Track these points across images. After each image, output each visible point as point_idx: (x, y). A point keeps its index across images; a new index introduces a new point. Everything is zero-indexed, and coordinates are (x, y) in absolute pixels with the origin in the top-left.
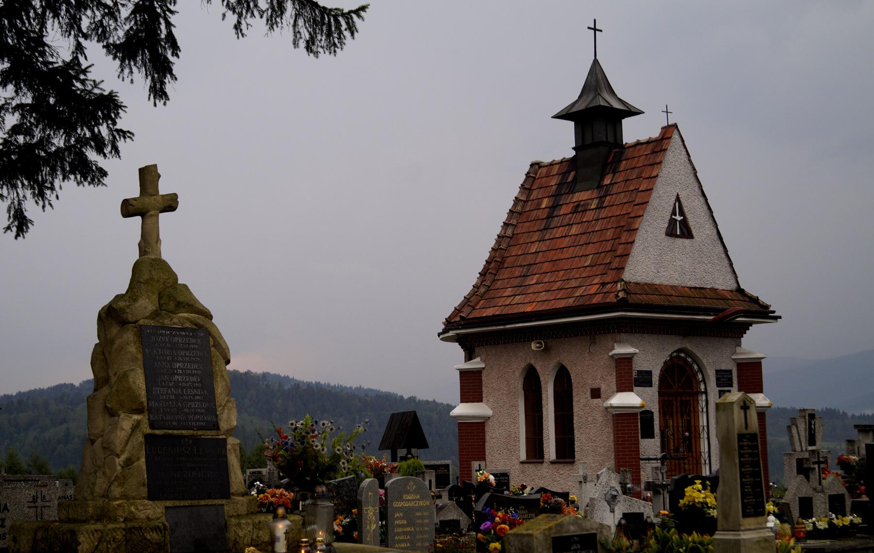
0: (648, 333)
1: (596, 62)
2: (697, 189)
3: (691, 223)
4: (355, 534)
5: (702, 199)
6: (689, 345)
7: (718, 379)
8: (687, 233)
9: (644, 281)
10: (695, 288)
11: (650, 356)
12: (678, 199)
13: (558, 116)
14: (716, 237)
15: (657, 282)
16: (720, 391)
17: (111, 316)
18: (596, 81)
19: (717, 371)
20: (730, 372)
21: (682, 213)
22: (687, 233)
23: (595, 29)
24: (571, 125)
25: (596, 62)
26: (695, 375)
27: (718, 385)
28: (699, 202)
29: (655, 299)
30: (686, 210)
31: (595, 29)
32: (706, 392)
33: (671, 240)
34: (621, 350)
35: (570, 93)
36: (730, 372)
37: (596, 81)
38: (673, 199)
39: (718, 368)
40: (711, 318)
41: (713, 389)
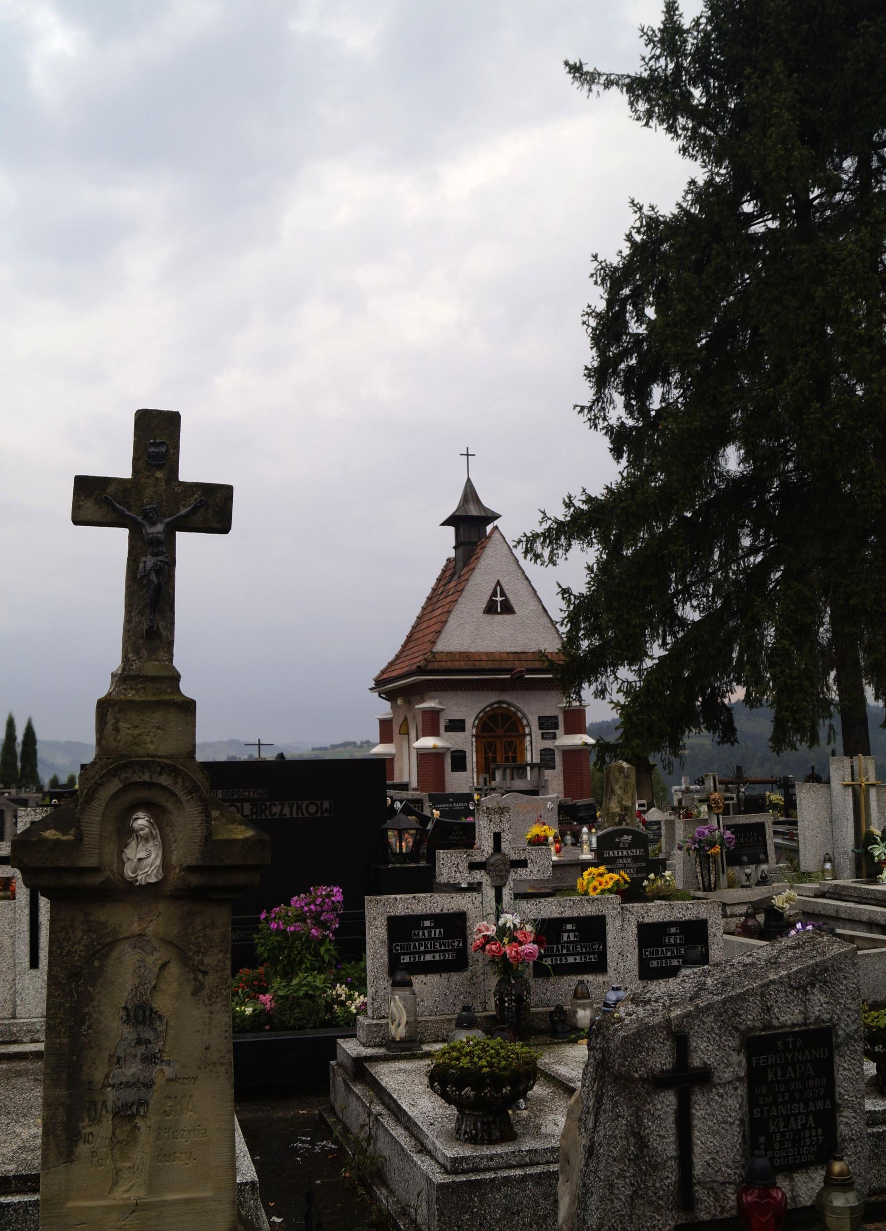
0: (461, 690)
1: (469, 480)
2: (520, 574)
3: (513, 602)
4: (762, 856)
5: (526, 582)
6: (507, 697)
7: (540, 724)
8: (507, 609)
9: (458, 650)
10: (516, 653)
11: (468, 708)
12: (498, 583)
13: (442, 524)
14: (542, 610)
15: (473, 650)
16: (543, 734)
17: (103, 706)
18: (470, 494)
19: (540, 718)
20: (556, 718)
21: (503, 594)
22: (507, 609)
23: (468, 455)
24: (451, 530)
25: (469, 480)
26: (520, 720)
27: (540, 729)
28: (522, 585)
29: (463, 665)
30: (507, 592)
31: (468, 455)
32: (530, 734)
33: (489, 617)
34: (430, 704)
35: (451, 506)
36: (556, 718)
37: (470, 494)
38: (493, 585)
39: (542, 715)
40: (551, 676)
41: (537, 732)
